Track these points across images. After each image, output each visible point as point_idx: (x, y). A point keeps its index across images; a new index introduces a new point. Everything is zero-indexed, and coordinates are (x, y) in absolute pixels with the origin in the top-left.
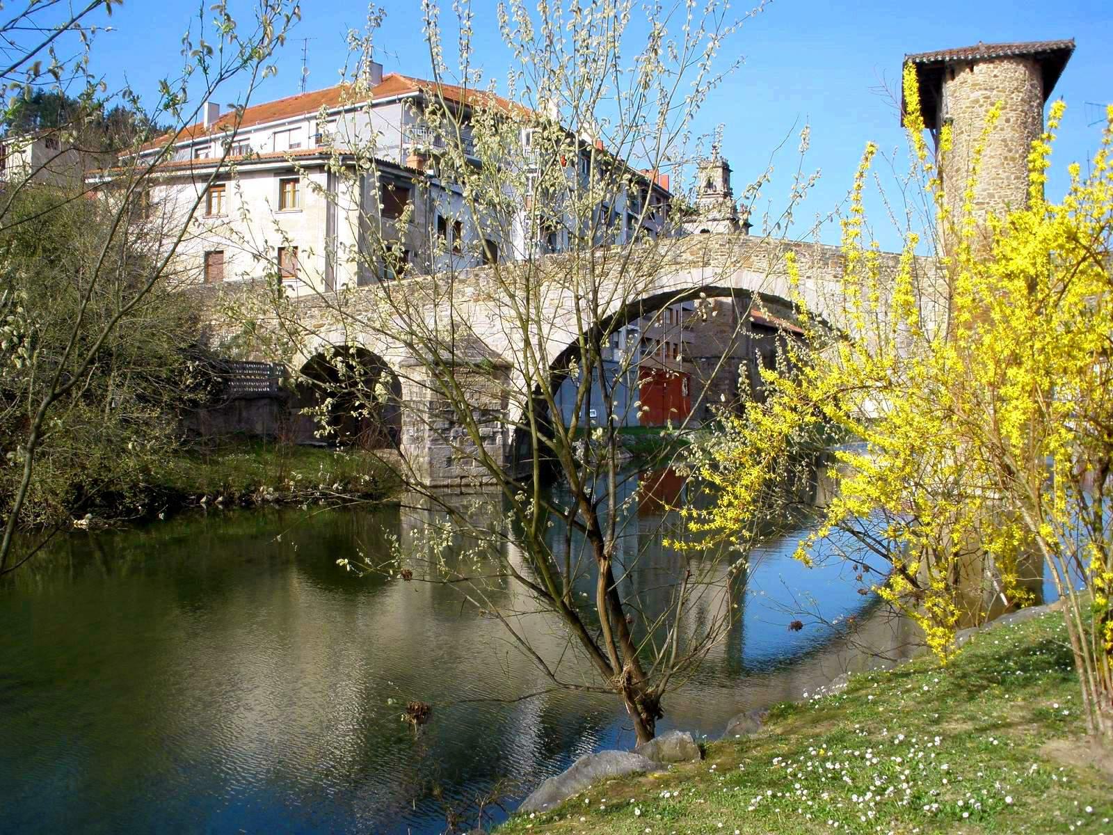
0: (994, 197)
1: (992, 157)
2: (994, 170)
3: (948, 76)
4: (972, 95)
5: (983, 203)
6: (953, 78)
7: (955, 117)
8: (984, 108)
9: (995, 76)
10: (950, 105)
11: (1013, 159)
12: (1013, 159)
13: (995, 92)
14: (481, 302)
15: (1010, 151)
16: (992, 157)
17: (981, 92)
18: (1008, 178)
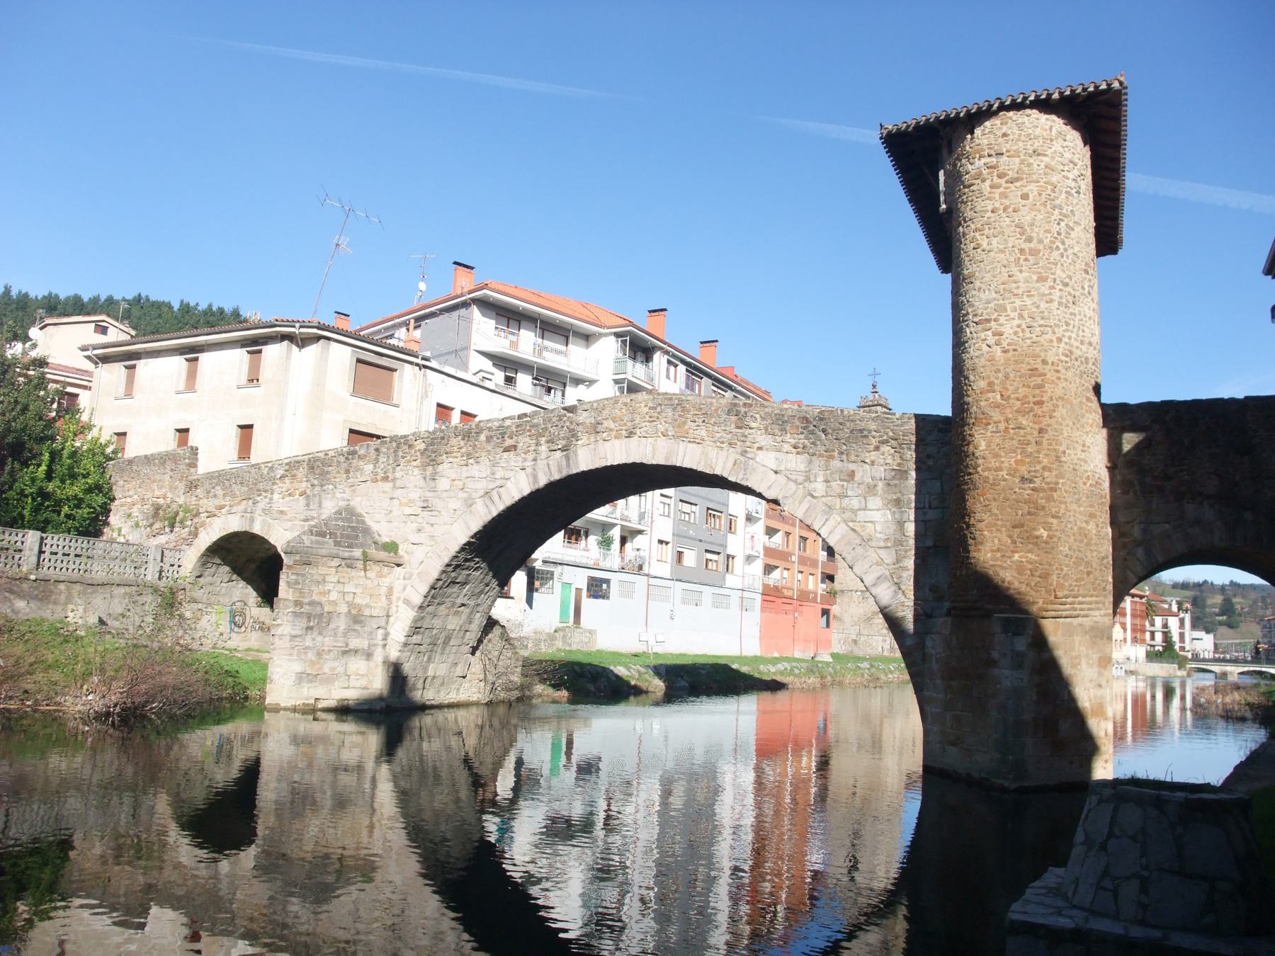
0: (1005, 310)
3: (945, 151)
8: (988, 183)
9: (1005, 135)
12: (1034, 252)
15: (1029, 240)
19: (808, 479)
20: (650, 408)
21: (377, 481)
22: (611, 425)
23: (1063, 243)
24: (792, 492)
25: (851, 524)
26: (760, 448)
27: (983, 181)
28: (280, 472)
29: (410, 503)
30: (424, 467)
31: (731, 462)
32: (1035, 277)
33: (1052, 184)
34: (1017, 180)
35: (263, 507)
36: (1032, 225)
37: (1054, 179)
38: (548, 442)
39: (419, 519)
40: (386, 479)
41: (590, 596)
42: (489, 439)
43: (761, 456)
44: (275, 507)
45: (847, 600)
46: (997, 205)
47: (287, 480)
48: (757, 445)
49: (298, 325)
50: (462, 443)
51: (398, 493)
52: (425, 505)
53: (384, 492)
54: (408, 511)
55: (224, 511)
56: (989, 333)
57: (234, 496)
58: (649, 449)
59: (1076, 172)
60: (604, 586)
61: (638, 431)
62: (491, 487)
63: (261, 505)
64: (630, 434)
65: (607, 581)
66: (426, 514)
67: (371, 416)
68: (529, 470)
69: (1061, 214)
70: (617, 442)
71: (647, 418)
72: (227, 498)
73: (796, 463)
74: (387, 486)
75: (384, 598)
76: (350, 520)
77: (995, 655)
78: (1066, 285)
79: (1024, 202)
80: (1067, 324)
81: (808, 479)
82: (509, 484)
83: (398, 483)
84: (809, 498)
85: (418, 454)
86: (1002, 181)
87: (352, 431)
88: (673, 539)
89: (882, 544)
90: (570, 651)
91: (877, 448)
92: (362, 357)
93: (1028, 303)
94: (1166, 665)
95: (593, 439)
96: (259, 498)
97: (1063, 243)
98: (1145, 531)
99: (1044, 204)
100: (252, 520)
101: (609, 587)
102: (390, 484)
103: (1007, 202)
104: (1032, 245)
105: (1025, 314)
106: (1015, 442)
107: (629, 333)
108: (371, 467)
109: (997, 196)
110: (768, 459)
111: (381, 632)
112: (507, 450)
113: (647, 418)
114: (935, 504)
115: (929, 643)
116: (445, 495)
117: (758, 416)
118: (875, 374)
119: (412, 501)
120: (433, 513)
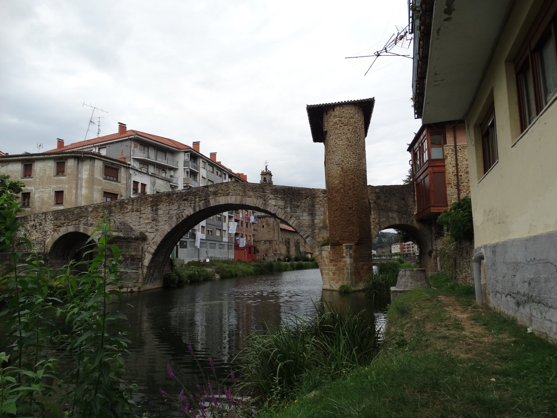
1: (343, 145)
2: (344, 150)
4: (334, 120)
5: (339, 164)
6: (327, 114)
7: (328, 130)
8: (339, 125)
9: (343, 112)
10: (326, 125)
11: (351, 146)
12: (351, 146)
13: (343, 119)
14: (135, 212)
16: (343, 145)
17: (337, 119)
18: (350, 153)
19: (285, 208)
20: (234, 187)
21: (133, 211)
22: (220, 191)
23: (358, 143)
24: (280, 212)
25: (298, 221)
26: (270, 199)
27: (338, 125)
28: (90, 209)
29: (148, 219)
30: (152, 206)
31: (261, 203)
32: (352, 153)
33: (356, 127)
34: (347, 125)
35: (84, 222)
36: (351, 138)
37: (356, 125)
38: (199, 197)
39: (152, 224)
40: (137, 211)
41: (180, 248)
42: (177, 197)
43: (270, 201)
44: (89, 222)
45: (259, 244)
46: (341, 132)
47: (94, 212)
48: (269, 198)
49: (82, 153)
50: (167, 198)
51: (142, 215)
52: (154, 219)
53: (136, 215)
54: (147, 221)
55: (65, 225)
56: (340, 168)
57: (69, 219)
58: (234, 199)
59: (361, 123)
60: (185, 244)
61: (230, 194)
62: (179, 212)
63: (83, 222)
64: (228, 195)
65: (186, 242)
66: (154, 222)
67: (111, 186)
68: (192, 207)
69: (358, 135)
70: (223, 197)
71: (233, 190)
72: (66, 220)
73: (281, 203)
74: (138, 213)
75: (141, 252)
76: (124, 225)
77: (344, 255)
78: (359, 155)
79: (348, 131)
80: (360, 166)
81: (285, 208)
82: (185, 211)
83: (142, 212)
84: (286, 213)
85: (150, 202)
86: (343, 125)
87: (105, 192)
88: (206, 226)
89: (308, 226)
90: (198, 264)
91: (305, 199)
92: (107, 165)
93: (350, 160)
94: (525, 237)
95: (215, 196)
96: (81, 219)
97: (358, 143)
98: (379, 221)
99: (354, 132)
100: (79, 227)
101: (186, 244)
102: (139, 213)
103: (344, 131)
104: (350, 144)
105: (349, 163)
106: (347, 198)
107: (190, 151)
108: (130, 207)
109: (341, 129)
110: (273, 202)
111: (140, 263)
112: (184, 200)
113: (233, 190)
114: (322, 214)
115: (323, 253)
116: (161, 215)
117: (269, 189)
118: (266, 163)
119: (148, 218)
120: (157, 222)
